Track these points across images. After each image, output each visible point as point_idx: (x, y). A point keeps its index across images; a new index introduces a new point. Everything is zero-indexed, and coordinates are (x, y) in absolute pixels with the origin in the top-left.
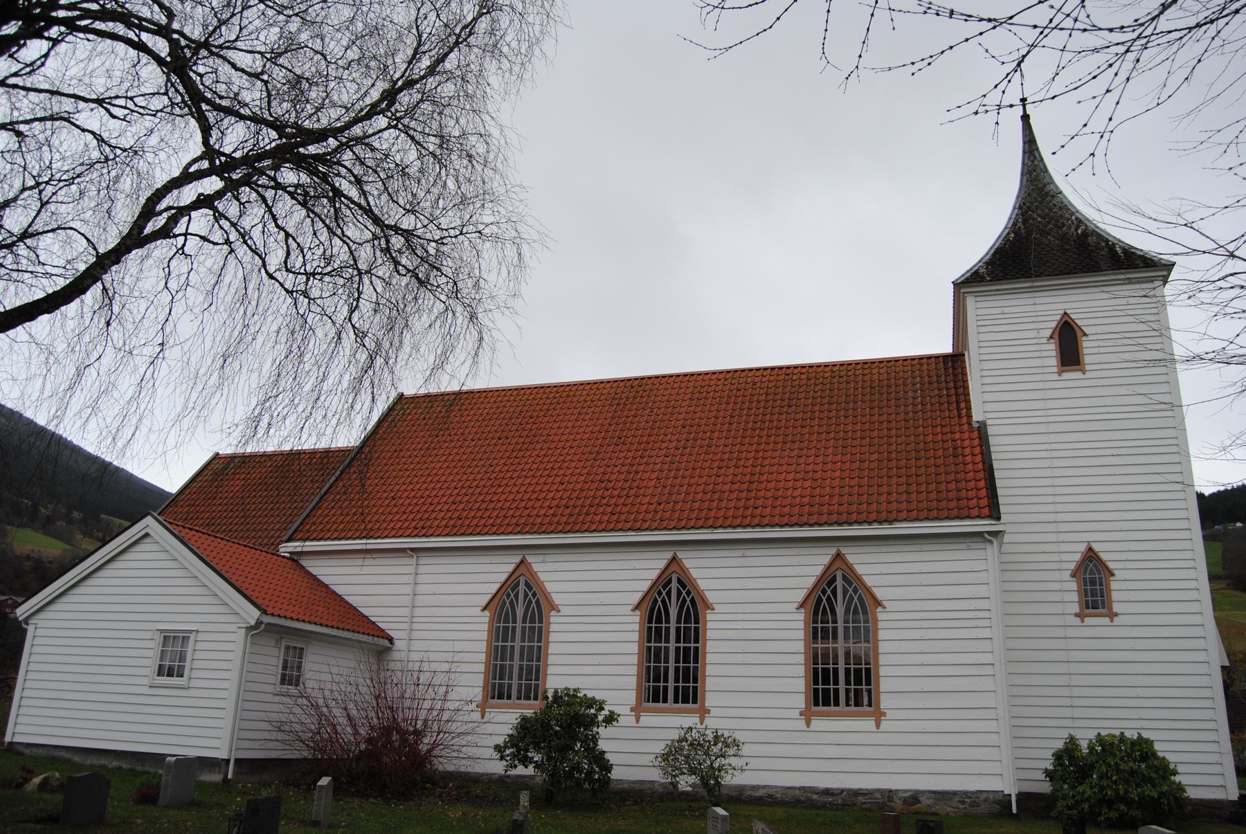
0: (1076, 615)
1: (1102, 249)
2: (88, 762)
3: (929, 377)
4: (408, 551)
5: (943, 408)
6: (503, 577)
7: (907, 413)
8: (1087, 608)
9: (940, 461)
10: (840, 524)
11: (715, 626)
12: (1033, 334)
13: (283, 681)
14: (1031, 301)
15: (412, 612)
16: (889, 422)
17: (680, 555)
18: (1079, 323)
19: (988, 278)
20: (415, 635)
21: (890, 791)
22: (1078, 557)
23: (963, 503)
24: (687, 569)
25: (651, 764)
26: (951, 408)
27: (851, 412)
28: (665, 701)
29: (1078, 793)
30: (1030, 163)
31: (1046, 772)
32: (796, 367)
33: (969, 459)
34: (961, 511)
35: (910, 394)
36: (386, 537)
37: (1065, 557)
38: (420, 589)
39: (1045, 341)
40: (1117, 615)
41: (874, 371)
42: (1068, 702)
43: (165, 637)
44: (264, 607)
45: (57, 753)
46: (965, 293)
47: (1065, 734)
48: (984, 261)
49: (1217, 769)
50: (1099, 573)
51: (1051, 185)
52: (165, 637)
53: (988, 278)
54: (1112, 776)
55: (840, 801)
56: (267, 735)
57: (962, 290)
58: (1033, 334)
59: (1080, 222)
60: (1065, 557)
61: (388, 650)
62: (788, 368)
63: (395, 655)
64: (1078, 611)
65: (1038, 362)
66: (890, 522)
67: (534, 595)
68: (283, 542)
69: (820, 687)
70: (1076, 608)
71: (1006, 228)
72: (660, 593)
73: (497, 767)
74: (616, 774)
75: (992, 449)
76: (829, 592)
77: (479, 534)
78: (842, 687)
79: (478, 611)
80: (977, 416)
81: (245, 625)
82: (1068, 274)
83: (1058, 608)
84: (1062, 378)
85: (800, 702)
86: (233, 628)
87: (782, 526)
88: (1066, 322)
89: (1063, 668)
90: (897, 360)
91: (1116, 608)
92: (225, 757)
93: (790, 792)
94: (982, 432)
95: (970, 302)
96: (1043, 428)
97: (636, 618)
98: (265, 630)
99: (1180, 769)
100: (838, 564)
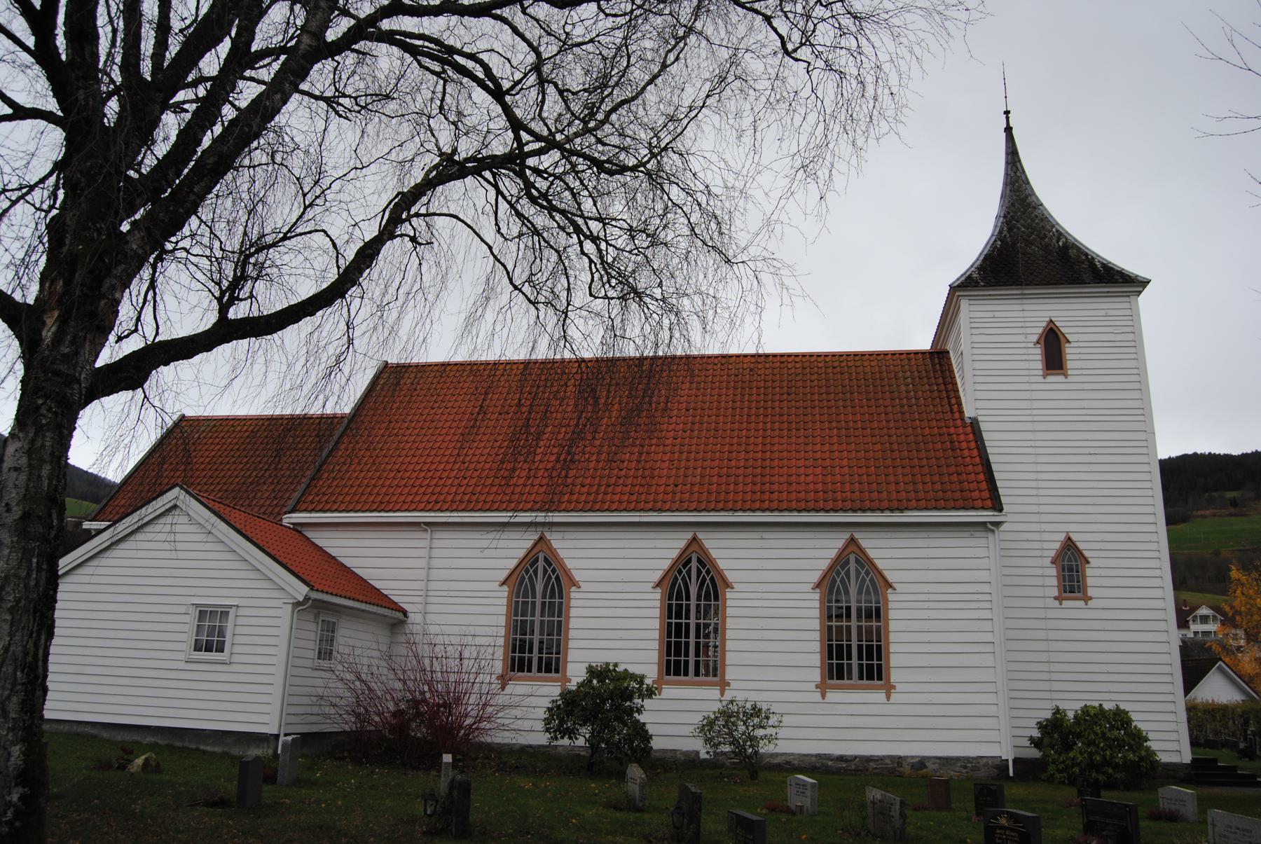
0: (1055, 598)
1: (1083, 263)
2: (119, 738)
3: (919, 372)
4: (422, 525)
5: (935, 403)
6: (521, 553)
7: (902, 406)
8: (1065, 592)
10: (854, 511)
11: (735, 603)
12: (1021, 338)
13: (198, 647)
14: (1020, 308)
16: (886, 414)
17: (700, 536)
18: (1063, 330)
19: (982, 284)
20: (430, 608)
21: (900, 757)
22: (1057, 546)
24: (707, 549)
25: (691, 735)
26: (943, 403)
27: (849, 403)
28: (686, 674)
31: (1032, 739)
32: (789, 355)
33: (966, 453)
34: (966, 502)
35: (903, 388)
36: (399, 510)
37: (1046, 545)
38: (435, 563)
39: (1032, 345)
40: (1091, 598)
41: (866, 364)
42: (1046, 676)
43: (200, 611)
44: (312, 583)
45: (81, 729)
46: (959, 296)
47: (1051, 705)
48: (976, 266)
49: (1174, 736)
51: (1033, 197)
52: (200, 611)
53: (982, 284)
54: (1099, 743)
56: (308, 710)
57: (957, 294)
58: (1021, 338)
59: (1060, 234)
60: (1046, 545)
61: (402, 623)
62: (782, 355)
64: (1057, 594)
66: (901, 510)
67: (554, 571)
68: (286, 513)
69: (672, 658)
70: (1055, 592)
71: (992, 235)
72: (680, 572)
73: (542, 739)
74: (656, 744)
75: (987, 444)
77: (497, 510)
79: (496, 586)
80: (969, 412)
81: (291, 601)
82: (1055, 284)
84: (1047, 380)
85: (816, 675)
86: (279, 603)
87: (799, 511)
89: (1043, 646)
90: (886, 354)
91: (1090, 592)
92: (276, 732)
94: (974, 425)
95: (964, 305)
96: (1029, 426)
98: (311, 607)
99: (1150, 736)
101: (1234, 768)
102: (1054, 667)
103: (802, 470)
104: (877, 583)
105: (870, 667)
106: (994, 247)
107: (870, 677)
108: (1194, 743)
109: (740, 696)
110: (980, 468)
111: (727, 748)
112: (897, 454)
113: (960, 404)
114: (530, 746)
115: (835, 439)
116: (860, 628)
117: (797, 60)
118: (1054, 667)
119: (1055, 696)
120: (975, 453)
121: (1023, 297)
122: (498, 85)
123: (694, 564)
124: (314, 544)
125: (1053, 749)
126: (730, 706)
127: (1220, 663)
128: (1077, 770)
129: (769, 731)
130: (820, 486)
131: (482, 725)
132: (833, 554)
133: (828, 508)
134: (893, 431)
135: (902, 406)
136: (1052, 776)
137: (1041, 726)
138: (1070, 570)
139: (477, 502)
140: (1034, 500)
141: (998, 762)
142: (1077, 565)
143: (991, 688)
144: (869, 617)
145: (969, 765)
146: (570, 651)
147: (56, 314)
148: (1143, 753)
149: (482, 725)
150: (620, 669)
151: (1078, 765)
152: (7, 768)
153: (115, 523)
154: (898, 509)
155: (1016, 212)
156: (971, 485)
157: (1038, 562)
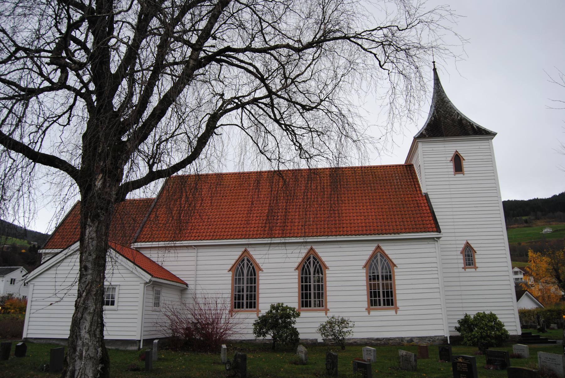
0: (463, 268)
5: (409, 187)
6: (237, 257)
7: (395, 189)
8: (467, 265)
9: (413, 209)
10: (379, 234)
12: (444, 159)
14: (443, 146)
15: (196, 273)
16: (389, 192)
18: (462, 155)
21: (402, 338)
22: (463, 246)
23: (425, 226)
28: (310, 306)
29: (472, 335)
30: (437, 89)
31: (456, 328)
37: (458, 246)
38: (199, 263)
39: (449, 161)
40: (477, 268)
41: (379, 171)
42: (460, 301)
45: (51, 342)
48: (424, 128)
49: (514, 324)
50: (471, 252)
55: (383, 343)
56: (152, 329)
57: (417, 140)
58: (444, 159)
59: (458, 114)
60: (458, 246)
61: (186, 289)
63: (189, 292)
64: (463, 266)
65: (446, 170)
66: (398, 233)
70: (463, 265)
72: (306, 263)
73: (252, 337)
74: (301, 337)
76: (375, 261)
77: (225, 239)
78: (382, 298)
79: (226, 272)
80: (424, 191)
81: (144, 282)
83: (456, 266)
85: (366, 305)
86: (138, 283)
87: (356, 235)
88: (457, 155)
91: (477, 265)
92: (139, 339)
93: (363, 340)
94: (426, 196)
95: (420, 145)
97: (297, 273)
99: (505, 324)
100: (246, 254)
101: (539, 336)
102: (463, 297)
103: (355, 218)
104: (389, 265)
105: (388, 300)
106: (431, 120)
107: (388, 305)
108: (523, 327)
109: (336, 315)
110: (430, 214)
111: (330, 337)
112: (395, 210)
113: (419, 187)
114: (244, 340)
115: (368, 204)
116: (383, 284)
117: (384, 69)
118: (463, 297)
119: (464, 309)
120: (428, 208)
121: (445, 141)
122: (262, 76)
123: (312, 260)
124: (145, 256)
125: (465, 331)
126: (333, 319)
127: (527, 292)
128: (476, 339)
129: (349, 329)
130: (363, 224)
131: (227, 332)
132: (370, 253)
133: (368, 233)
134: (392, 200)
135: (395, 189)
136: (466, 342)
137: (459, 322)
138: (469, 256)
139: (217, 235)
140: (453, 227)
141: (443, 338)
142: (471, 254)
143: (439, 307)
144: (387, 279)
145: (431, 340)
146: (260, 299)
147: (101, 175)
148: (503, 331)
149: (227, 332)
150: (284, 305)
151: (476, 337)
152: (97, 356)
153: (64, 250)
154: (397, 233)
155: (439, 105)
156: (427, 222)
157: (455, 253)
